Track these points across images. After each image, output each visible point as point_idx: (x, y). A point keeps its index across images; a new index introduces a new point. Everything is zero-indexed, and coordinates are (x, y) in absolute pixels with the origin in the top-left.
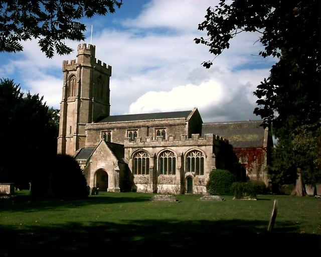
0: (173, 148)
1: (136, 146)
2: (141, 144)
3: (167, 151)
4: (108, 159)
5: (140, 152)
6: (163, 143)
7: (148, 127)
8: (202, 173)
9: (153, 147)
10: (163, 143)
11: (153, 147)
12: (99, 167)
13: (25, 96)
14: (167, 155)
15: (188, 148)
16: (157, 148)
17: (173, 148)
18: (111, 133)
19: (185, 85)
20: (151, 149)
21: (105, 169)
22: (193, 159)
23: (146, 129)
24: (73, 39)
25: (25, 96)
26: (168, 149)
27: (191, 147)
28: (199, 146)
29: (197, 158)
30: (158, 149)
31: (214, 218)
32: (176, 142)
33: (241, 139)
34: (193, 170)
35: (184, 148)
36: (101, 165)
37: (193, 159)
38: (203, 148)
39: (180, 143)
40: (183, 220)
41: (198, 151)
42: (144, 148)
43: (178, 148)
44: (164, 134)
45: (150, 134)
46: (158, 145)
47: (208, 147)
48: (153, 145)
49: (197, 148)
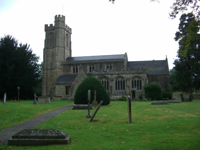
1: (100, 74)
2: (103, 73)
6: (117, 72)
9: (111, 75)
10: (117, 72)
11: (111, 75)
14: (120, 79)
15: (132, 75)
17: (124, 75)
18: (78, 67)
20: (110, 76)
22: (135, 81)
24: (45, 31)
26: (120, 75)
27: (134, 75)
28: (138, 74)
29: (121, 81)
30: (114, 76)
31: (57, 146)
32: (126, 72)
33: (154, 70)
35: (130, 75)
38: (141, 75)
39: (128, 72)
40: (61, 145)
41: (139, 77)
42: (105, 75)
43: (126, 75)
44: (111, 67)
45: (103, 67)
46: (114, 73)
47: (144, 74)
48: (111, 73)
49: (137, 75)
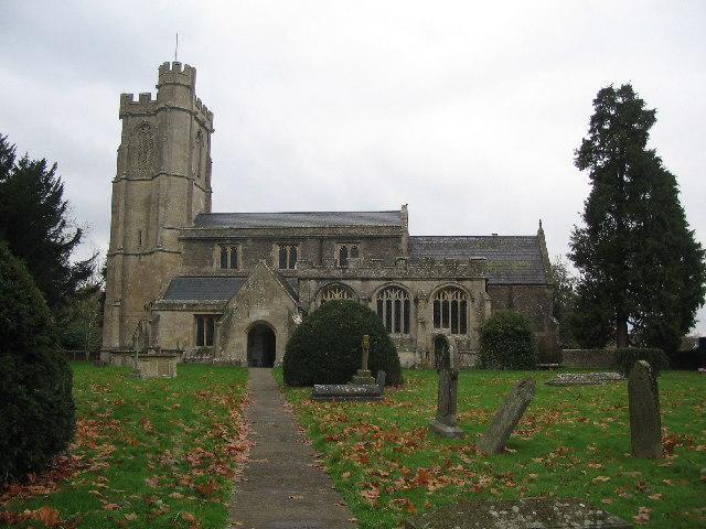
0: (405, 283)
2: (336, 273)
3: (391, 288)
4: (277, 301)
5: (391, 288)
6: (383, 273)
7: (322, 239)
8: (464, 331)
9: (363, 279)
11: (363, 279)
12: (248, 321)
13: (647, 148)
16: (372, 282)
18: (240, 248)
19: (585, 156)
21: (270, 321)
22: (446, 303)
23: (313, 244)
25: (647, 148)
27: (442, 282)
28: (458, 280)
29: (455, 303)
34: (446, 326)
36: (260, 313)
37: (446, 303)
42: (343, 282)
48: (363, 275)
49: (455, 284)
